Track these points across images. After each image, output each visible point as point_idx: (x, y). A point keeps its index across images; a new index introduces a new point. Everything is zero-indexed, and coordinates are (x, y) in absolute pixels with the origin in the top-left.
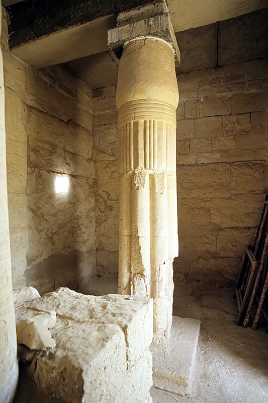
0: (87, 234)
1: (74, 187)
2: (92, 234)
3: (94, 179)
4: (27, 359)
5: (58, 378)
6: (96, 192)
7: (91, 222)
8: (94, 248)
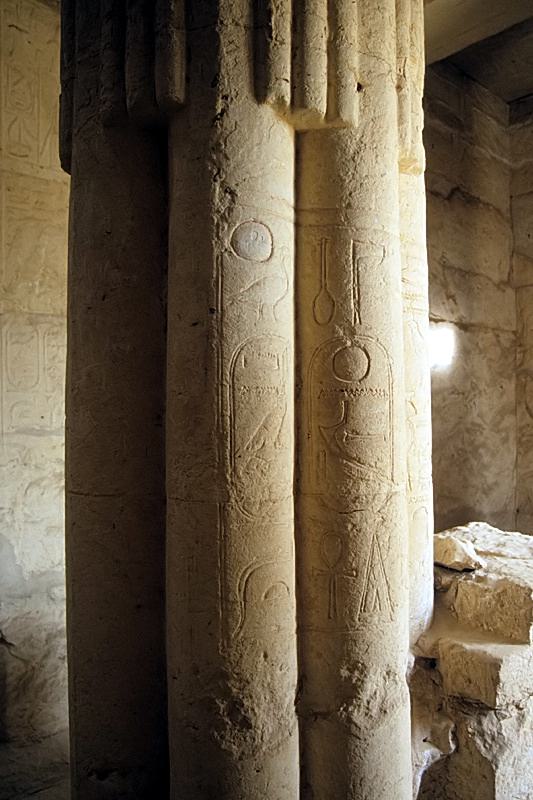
0: (494, 470)
1: (465, 352)
2: (506, 473)
3: (514, 333)
4: (443, 582)
5: (494, 602)
6: (521, 365)
7: (505, 440)
8: (512, 508)
